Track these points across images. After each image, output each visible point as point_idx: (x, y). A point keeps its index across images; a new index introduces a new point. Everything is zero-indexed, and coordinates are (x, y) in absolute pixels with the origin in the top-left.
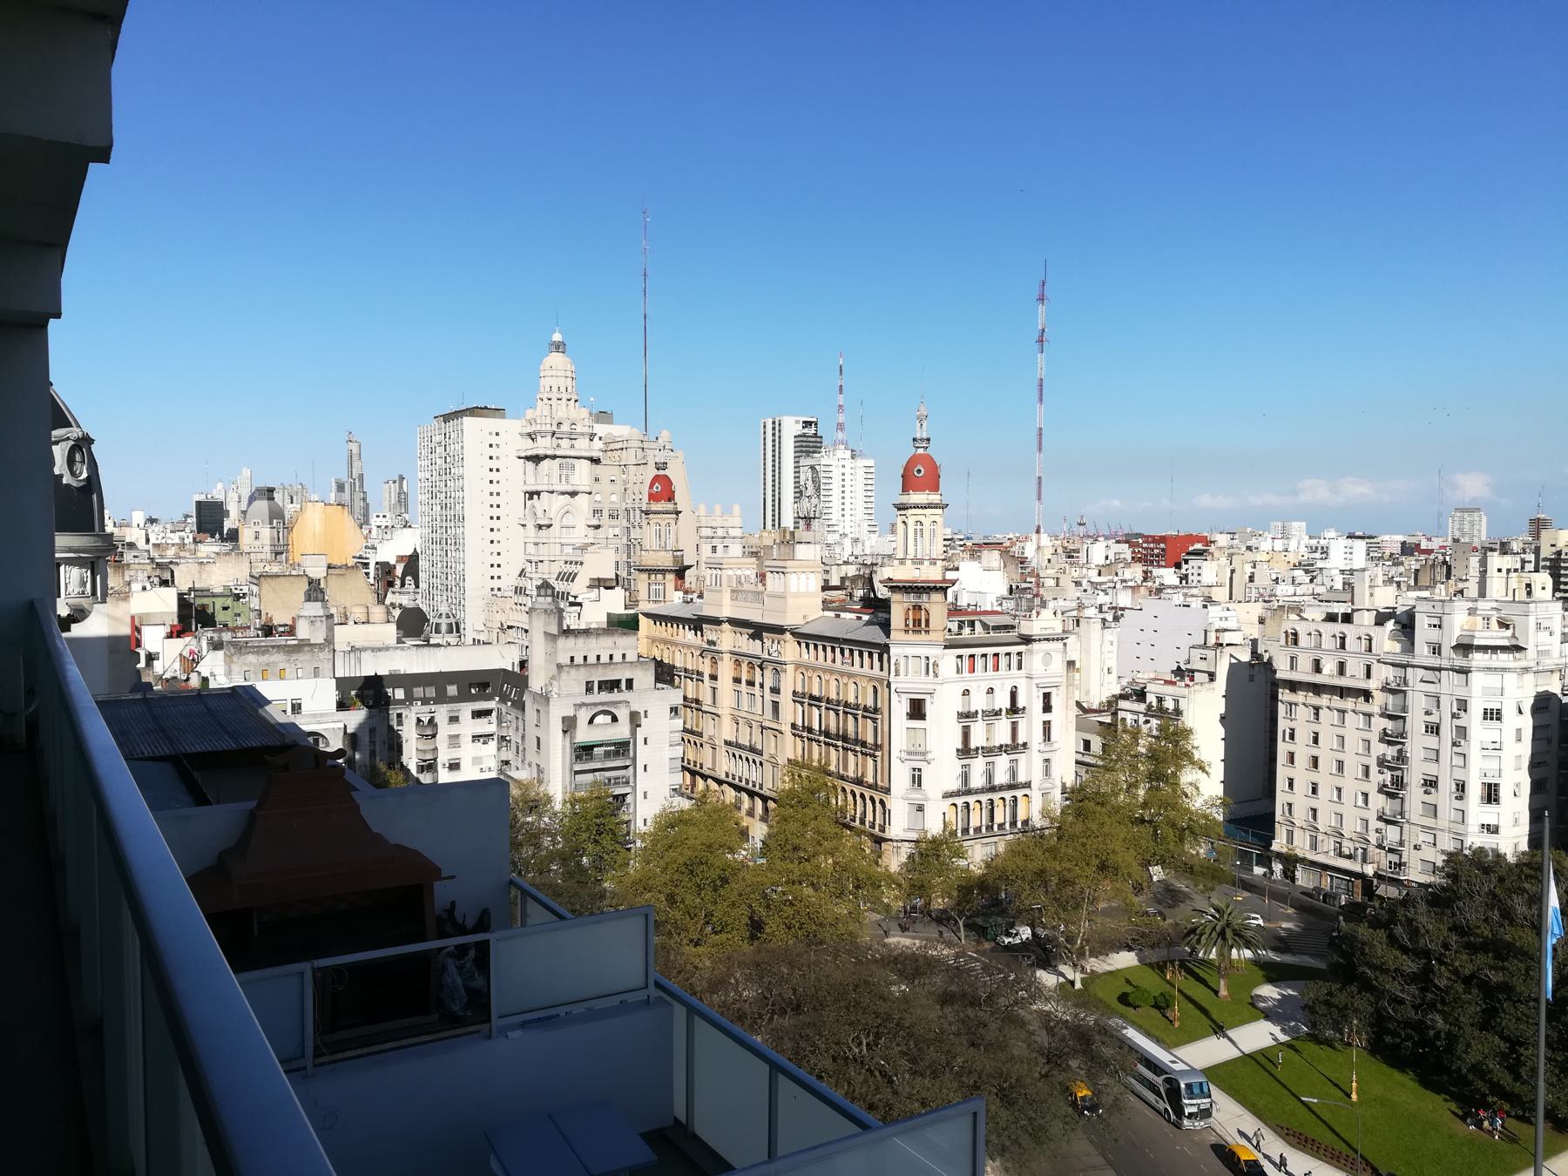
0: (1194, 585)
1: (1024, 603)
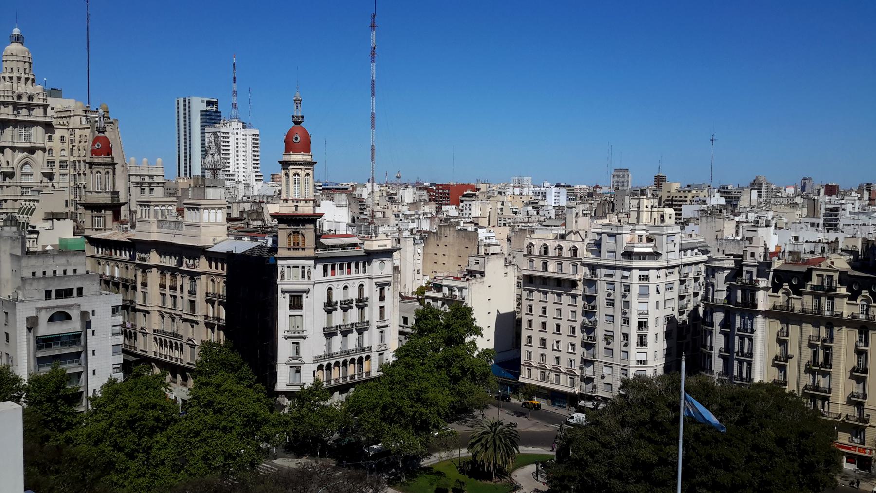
0: (467, 216)
1: (363, 228)
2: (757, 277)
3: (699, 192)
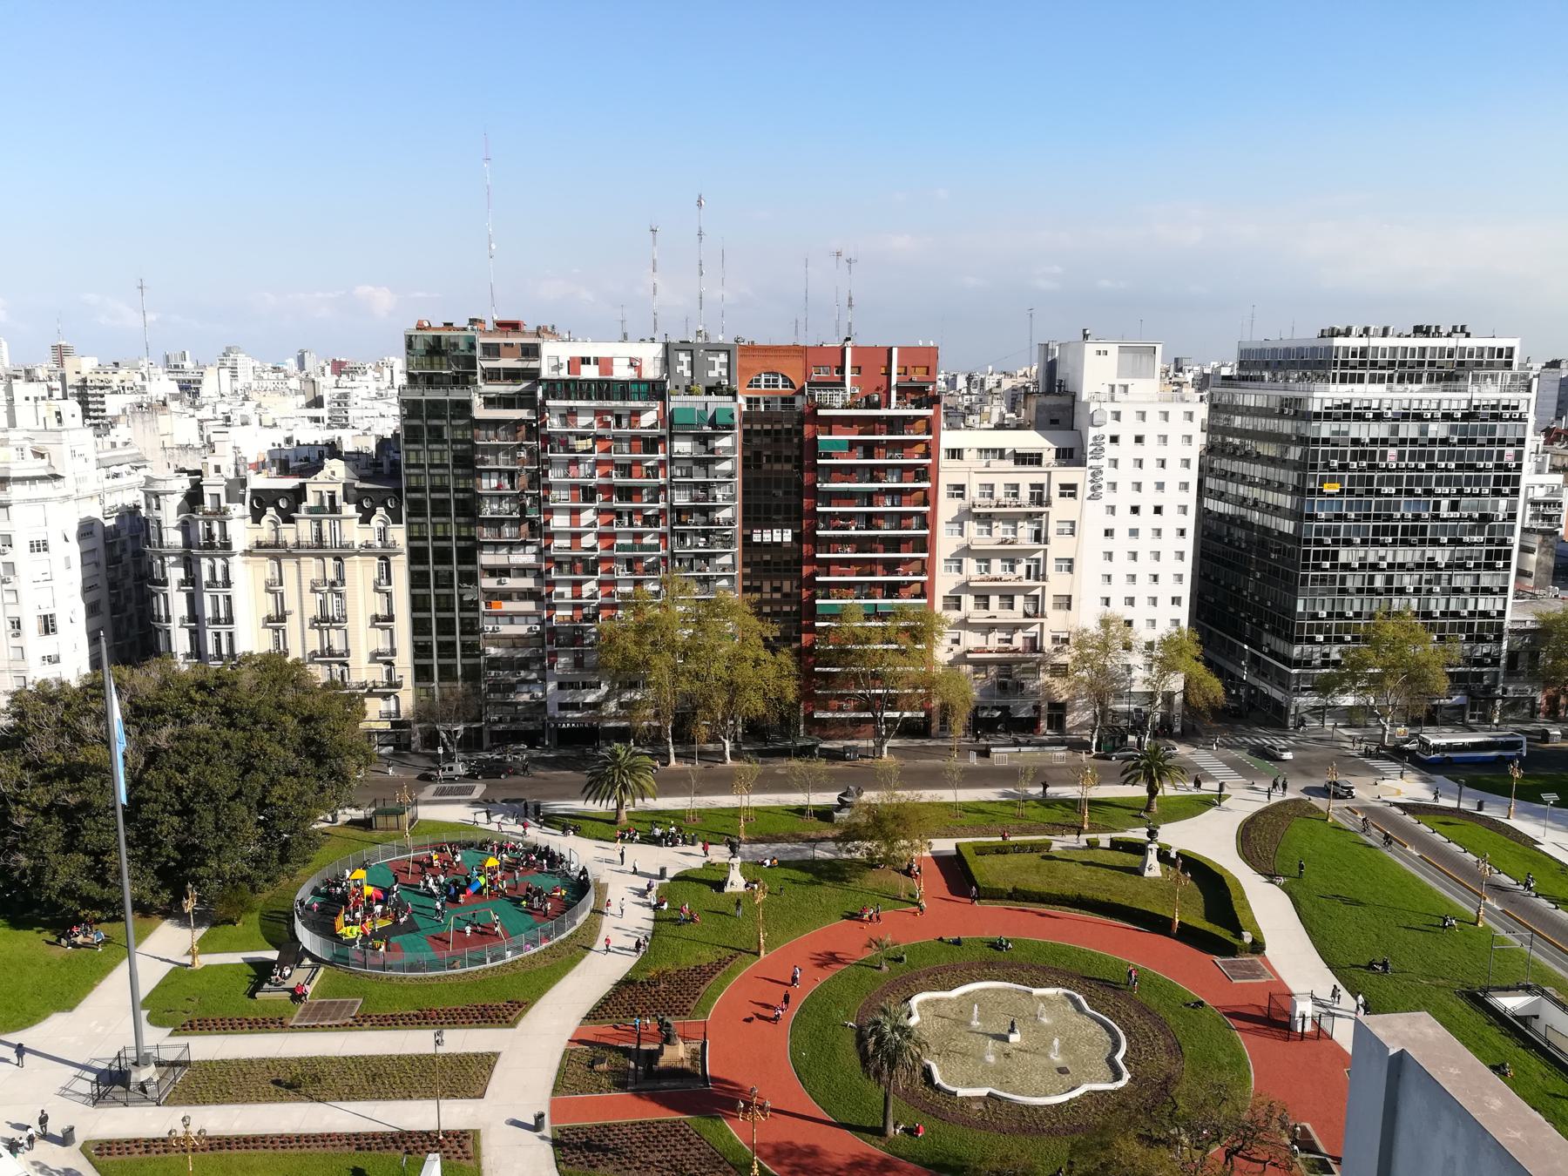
2: (228, 501)
3: (133, 372)
